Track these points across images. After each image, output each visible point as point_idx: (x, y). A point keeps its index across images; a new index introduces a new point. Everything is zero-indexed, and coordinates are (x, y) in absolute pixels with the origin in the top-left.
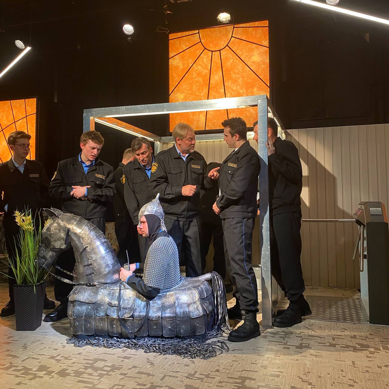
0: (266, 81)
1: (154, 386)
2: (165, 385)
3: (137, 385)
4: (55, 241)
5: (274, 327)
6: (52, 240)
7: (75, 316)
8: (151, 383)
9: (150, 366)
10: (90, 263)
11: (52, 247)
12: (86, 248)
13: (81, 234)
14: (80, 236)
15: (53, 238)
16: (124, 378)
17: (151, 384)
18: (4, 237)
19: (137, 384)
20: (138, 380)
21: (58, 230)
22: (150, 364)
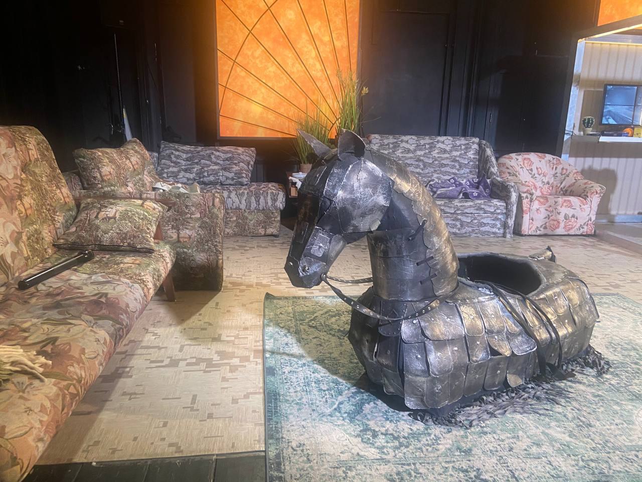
0: (321, 4)
1: (175, 360)
2: (189, 357)
3: (150, 363)
4: (363, 215)
5: (604, 300)
6: (355, 213)
7: (437, 373)
8: (168, 357)
9: (154, 337)
10: (428, 255)
11: (350, 229)
12: (424, 223)
13: (412, 195)
14: (410, 197)
15: (359, 208)
16: (125, 358)
17: (169, 359)
18: (510, 225)
19: (149, 362)
20: (148, 357)
21: (370, 188)
22: (152, 334)
